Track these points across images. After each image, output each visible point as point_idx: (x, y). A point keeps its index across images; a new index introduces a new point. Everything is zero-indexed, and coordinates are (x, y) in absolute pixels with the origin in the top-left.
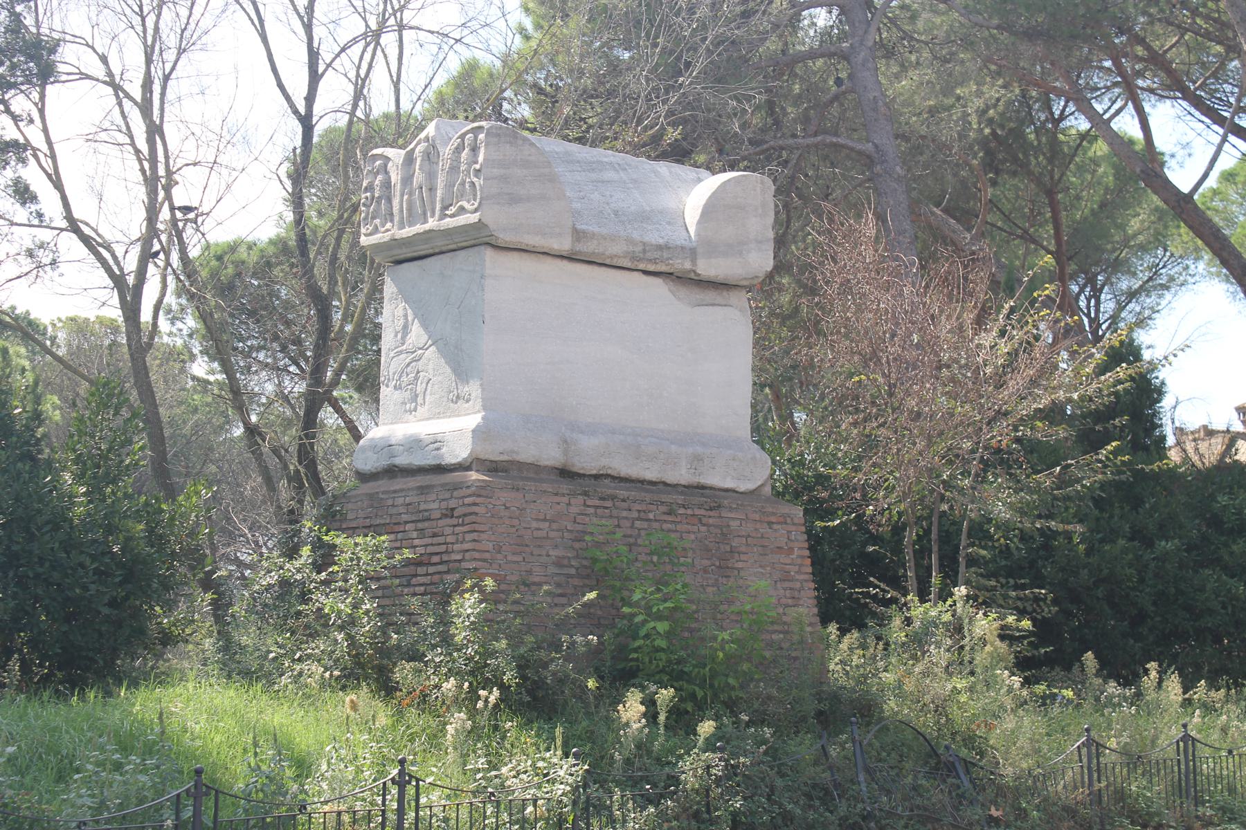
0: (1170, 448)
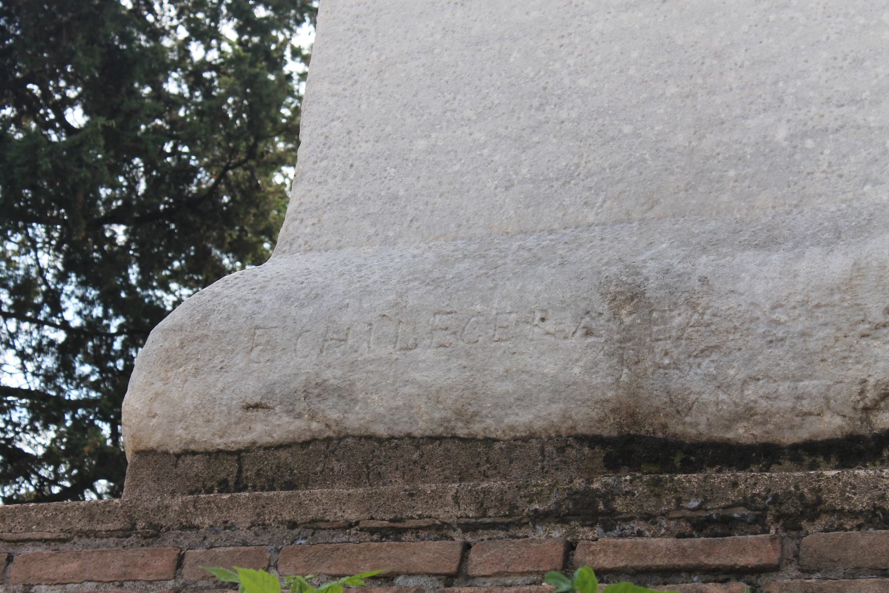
0: (62, 277)
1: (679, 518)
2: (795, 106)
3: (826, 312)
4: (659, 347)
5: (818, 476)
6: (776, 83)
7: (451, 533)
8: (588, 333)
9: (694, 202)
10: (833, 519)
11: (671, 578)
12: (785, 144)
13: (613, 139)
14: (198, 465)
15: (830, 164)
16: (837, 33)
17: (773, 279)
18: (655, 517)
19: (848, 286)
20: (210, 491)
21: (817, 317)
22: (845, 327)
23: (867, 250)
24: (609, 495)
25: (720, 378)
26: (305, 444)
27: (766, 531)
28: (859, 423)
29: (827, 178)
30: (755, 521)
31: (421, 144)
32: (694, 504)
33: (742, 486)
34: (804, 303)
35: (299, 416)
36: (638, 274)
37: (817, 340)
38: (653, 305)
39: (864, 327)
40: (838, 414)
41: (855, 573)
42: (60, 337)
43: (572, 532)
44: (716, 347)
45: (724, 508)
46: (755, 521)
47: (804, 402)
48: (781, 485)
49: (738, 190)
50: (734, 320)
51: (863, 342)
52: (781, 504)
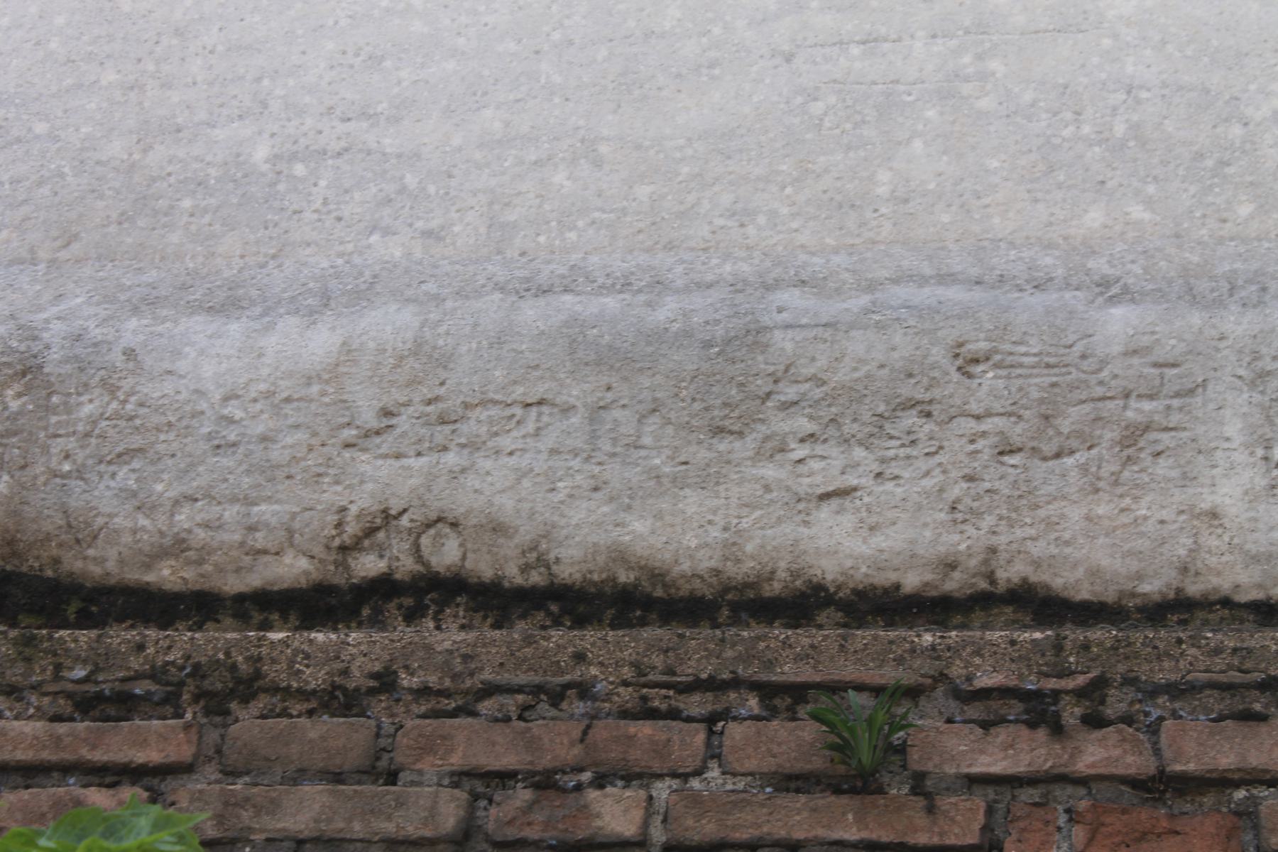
1: (56, 693)
2: (283, 115)
3: (299, 409)
4: (57, 446)
5: (259, 639)
6: (259, 80)
7: (372, 683)
9: (129, 240)
10: (274, 700)
11: (36, 780)
12: (265, 167)
13: (19, 140)
15: (325, 202)
16: (350, 17)
17: (229, 358)
18: (21, 690)
19: (332, 373)
21: (286, 416)
22: (324, 431)
23: (363, 325)
25: (142, 496)
28: (332, 568)
29: (320, 220)
30: (165, 701)
32: (80, 673)
33: (151, 651)
34: (269, 395)
36: (35, 338)
37: (283, 447)
38: (53, 384)
40: (304, 554)
41: (299, 776)
44: (140, 450)
45: (124, 680)
46: (165, 701)
47: (258, 535)
48: (206, 650)
49: (193, 228)
50: (169, 413)
51: (347, 454)
52: (204, 677)
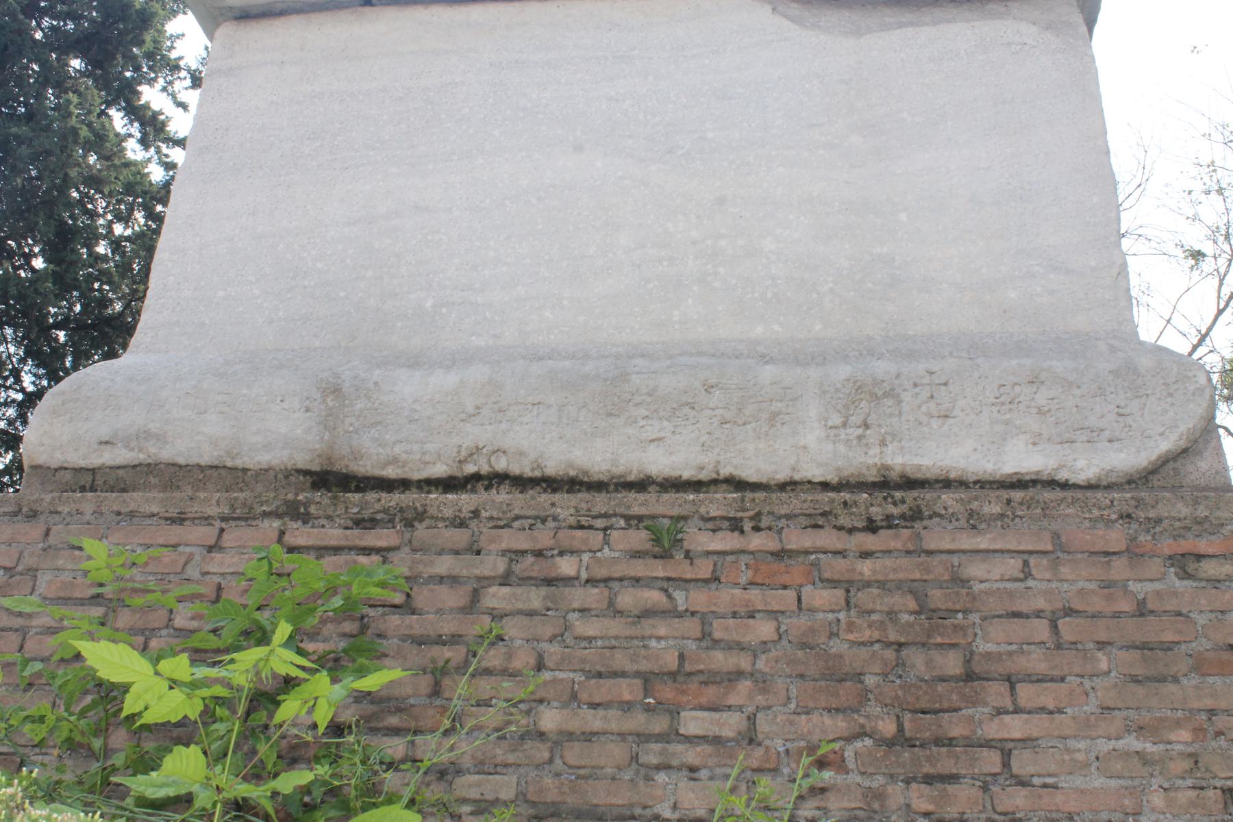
0: (23, 361)
4: (347, 421)
8: (308, 410)
14: (68, 476)
20: (74, 491)
24: (306, 504)
26: (135, 467)
27: (394, 527)
31: (221, 294)
32: (355, 510)
34: (431, 400)
35: (132, 450)
39: (463, 416)
41: (441, 552)
42: (19, 397)
43: (284, 524)
